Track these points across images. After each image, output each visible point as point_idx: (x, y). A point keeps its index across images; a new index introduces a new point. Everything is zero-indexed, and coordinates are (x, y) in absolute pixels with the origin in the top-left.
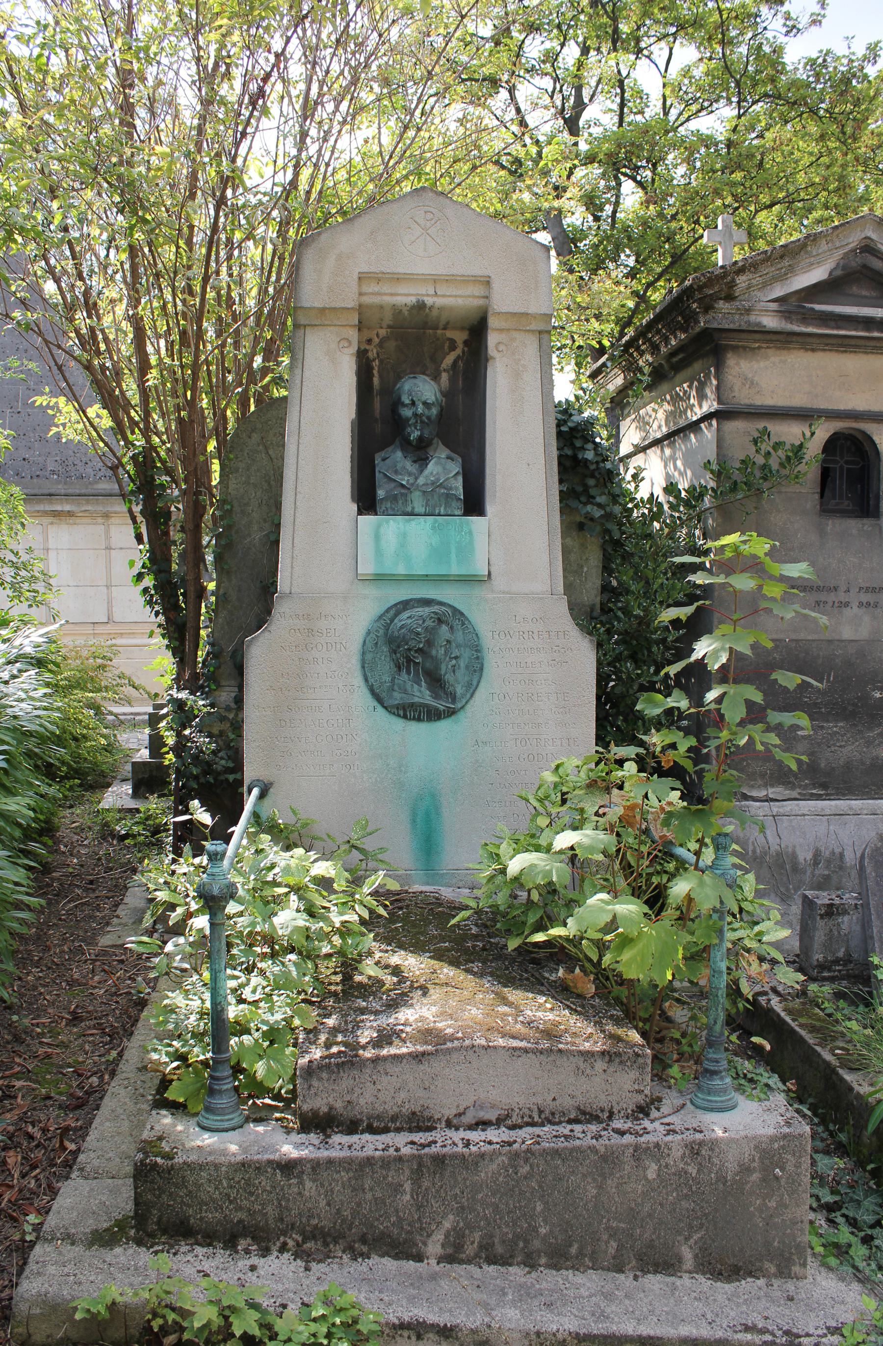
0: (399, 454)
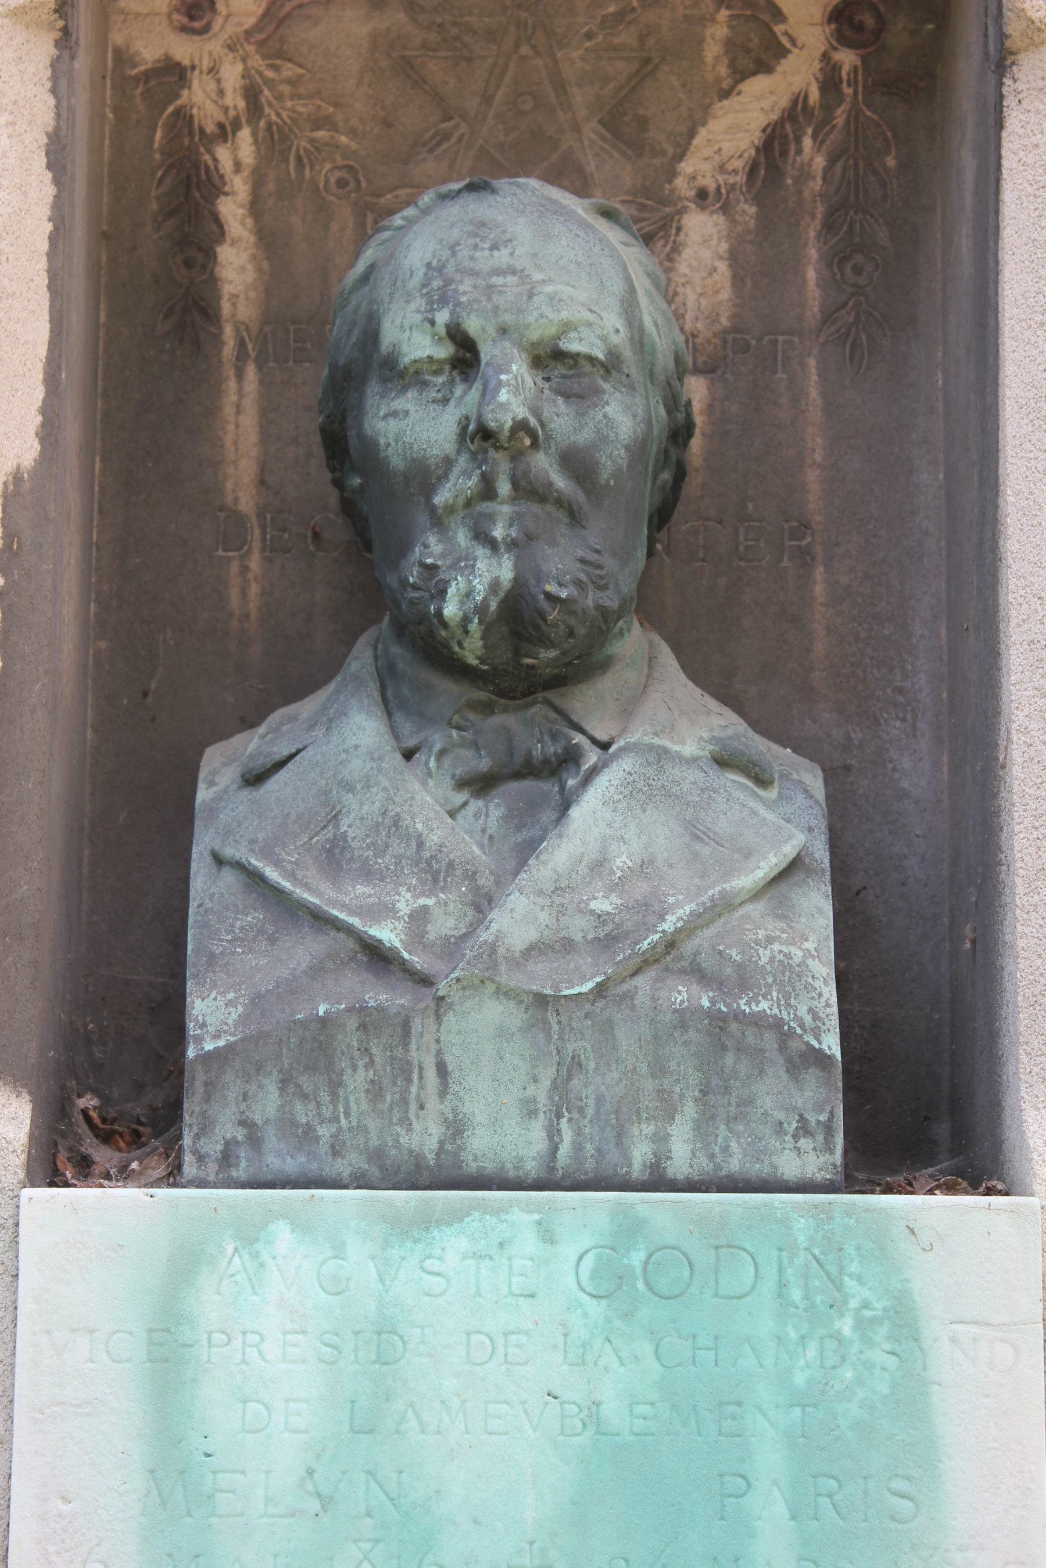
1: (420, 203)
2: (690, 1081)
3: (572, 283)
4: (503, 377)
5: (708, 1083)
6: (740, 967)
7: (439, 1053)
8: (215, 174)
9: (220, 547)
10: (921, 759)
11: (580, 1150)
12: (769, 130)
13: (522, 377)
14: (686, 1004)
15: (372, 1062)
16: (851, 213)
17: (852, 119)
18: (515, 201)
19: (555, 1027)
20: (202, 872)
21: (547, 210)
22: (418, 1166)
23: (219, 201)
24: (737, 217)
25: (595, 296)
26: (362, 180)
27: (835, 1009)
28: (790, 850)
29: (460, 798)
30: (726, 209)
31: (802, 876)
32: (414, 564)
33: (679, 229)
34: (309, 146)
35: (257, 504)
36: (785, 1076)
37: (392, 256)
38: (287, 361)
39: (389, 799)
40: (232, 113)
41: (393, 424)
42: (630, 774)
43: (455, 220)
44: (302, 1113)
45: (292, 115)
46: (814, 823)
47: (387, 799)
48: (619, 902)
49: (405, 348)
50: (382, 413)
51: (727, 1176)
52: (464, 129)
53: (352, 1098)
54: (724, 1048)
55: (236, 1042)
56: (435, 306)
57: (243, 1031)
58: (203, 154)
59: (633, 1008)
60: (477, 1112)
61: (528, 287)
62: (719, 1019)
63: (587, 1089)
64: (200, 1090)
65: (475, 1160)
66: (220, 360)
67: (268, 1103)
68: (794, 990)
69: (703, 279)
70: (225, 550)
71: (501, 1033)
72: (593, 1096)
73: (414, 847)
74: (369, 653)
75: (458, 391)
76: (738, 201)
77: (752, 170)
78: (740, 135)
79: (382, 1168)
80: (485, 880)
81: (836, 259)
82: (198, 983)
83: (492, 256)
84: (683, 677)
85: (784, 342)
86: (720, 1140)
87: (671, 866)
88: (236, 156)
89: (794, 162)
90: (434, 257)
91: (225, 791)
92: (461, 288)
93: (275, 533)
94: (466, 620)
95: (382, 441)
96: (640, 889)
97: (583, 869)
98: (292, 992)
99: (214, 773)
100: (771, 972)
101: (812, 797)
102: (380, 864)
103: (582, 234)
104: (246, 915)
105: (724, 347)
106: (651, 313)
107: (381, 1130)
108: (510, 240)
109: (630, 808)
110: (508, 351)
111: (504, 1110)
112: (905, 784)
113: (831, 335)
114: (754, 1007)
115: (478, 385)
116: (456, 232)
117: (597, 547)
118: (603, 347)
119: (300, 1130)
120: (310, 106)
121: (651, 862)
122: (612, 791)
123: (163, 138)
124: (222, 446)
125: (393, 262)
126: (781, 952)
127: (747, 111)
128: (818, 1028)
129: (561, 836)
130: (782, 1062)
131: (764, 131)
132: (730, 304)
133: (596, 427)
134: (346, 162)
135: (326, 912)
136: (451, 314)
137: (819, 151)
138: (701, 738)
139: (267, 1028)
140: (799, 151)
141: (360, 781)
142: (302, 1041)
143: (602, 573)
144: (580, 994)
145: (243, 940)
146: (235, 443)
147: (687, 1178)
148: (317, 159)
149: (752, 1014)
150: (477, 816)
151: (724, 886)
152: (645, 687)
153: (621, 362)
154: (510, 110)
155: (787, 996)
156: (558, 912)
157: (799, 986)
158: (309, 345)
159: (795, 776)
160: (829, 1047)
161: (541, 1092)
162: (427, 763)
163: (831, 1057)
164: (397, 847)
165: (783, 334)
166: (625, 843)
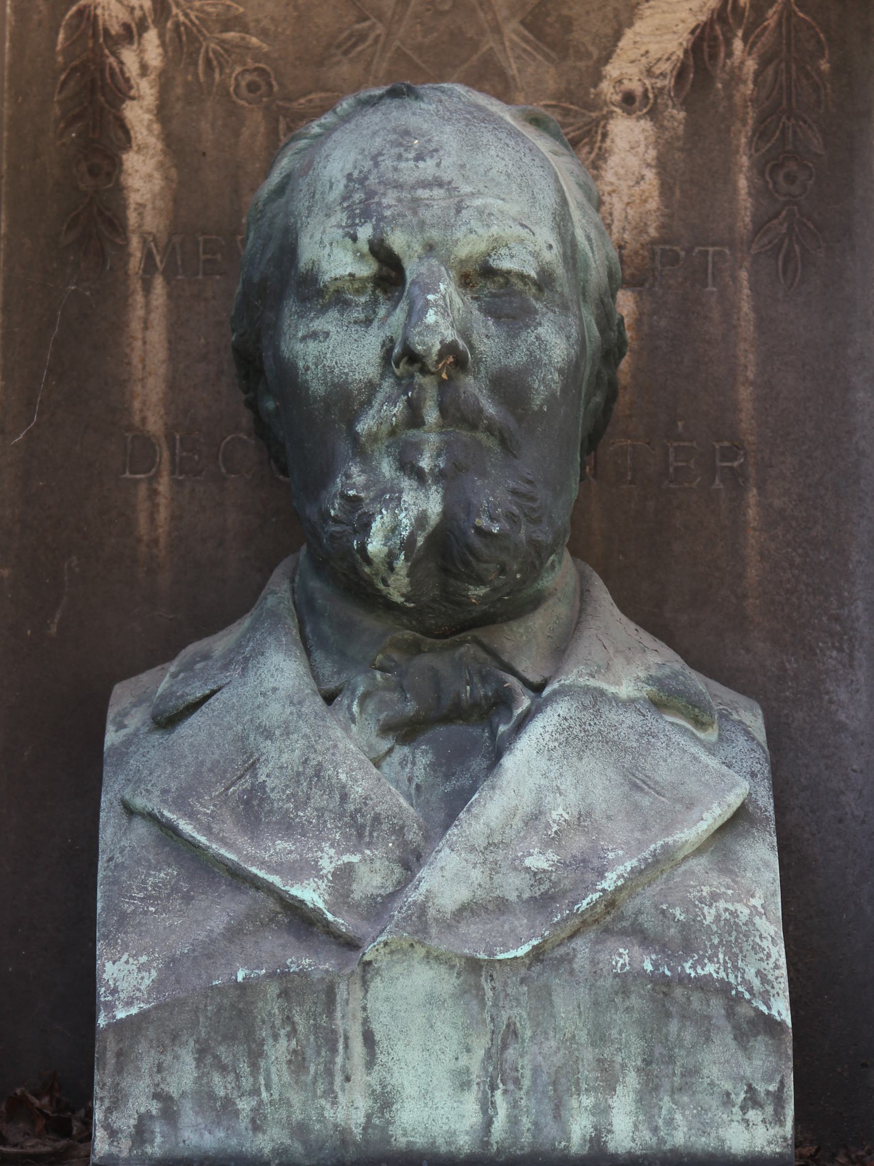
0: (282, 670)
1: (338, 110)
2: (632, 1049)
3: (503, 196)
4: (431, 297)
5: (651, 1053)
6: (684, 927)
7: (366, 1021)
8: (120, 77)
9: (127, 470)
10: (858, 691)
11: (516, 1124)
12: (698, 31)
13: (450, 297)
14: (628, 968)
15: (294, 1031)
16: (784, 119)
17: (784, 20)
18: (440, 108)
19: (490, 994)
20: (112, 821)
21: (474, 117)
22: (343, 1141)
23: (124, 106)
24: (666, 123)
25: (526, 210)
26: (274, 83)
27: (784, 971)
28: (734, 800)
29: (384, 745)
30: (653, 114)
31: (747, 826)
32: (335, 495)
33: (605, 135)
34: (218, 48)
35: (166, 424)
36: (732, 1044)
37: (310, 165)
38: (197, 274)
39: (310, 747)
40: (138, 13)
41: (312, 347)
42: (566, 719)
43: (377, 128)
44: (220, 1085)
45: (201, 15)
46: (757, 767)
47: (308, 747)
48: (556, 858)
49: (325, 266)
50: (300, 334)
51: (671, 1151)
52: (380, 29)
53: (273, 1069)
54: (668, 1015)
55: (149, 1010)
56: (357, 221)
57: (157, 998)
58: (108, 57)
59: (572, 972)
60: (405, 1083)
61: (457, 200)
62: (663, 984)
63: (524, 1058)
64: (111, 1060)
65: (404, 1135)
66: (126, 273)
67: (184, 1075)
68: (741, 952)
69: (630, 187)
70: (133, 472)
71: (432, 1000)
72: (529, 1067)
73: (338, 799)
74: (286, 585)
75: (382, 312)
76: (667, 106)
77: (681, 75)
78: (669, 36)
79: (305, 1143)
80: (413, 835)
81: (769, 166)
82: (108, 945)
83: (417, 167)
84: (616, 611)
85: (715, 254)
86: (664, 1112)
87: (609, 818)
88: (142, 59)
89: (725, 65)
90: (355, 168)
91: (135, 734)
92: (385, 201)
93: (184, 454)
94: (391, 557)
95: (301, 364)
96: (578, 844)
97: (517, 822)
98: (209, 956)
99: (125, 714)
100: (716, 932)
101: (753, 739)
102: (301, 817)
103: (512, 143)
104: (159, 871)
105: (653, 259)
106: (582, 227)
107: (304, 1103)
108: (436, 150)
109: (565, 756)
110: (435, 269)
111: (435, 1082)
112: (842, 717)
113: (763, 247)
114: (699, 971)
115: (403, 305)
116: (378, 141)
117: (530, 477)
118: (535, 265)
119: (219, 1104)
120: (220, 6)
121: (589, 814)
122: (547, 739)
123: (66, 39)
124: (129, 363)
125: (311, 172)
126: (726, 910)
127: (675, 12)
128: (767, 992)
129: (493, 788)
130: (729, 1029)
131: (693, 32)
132: (658, 213)
133: (528, 350)
134: (257, 65)
135: (244, 870)
136: (374, 229)
137: (749, 54)
138: (638, 677)
139: (182, 995)
140: (730, 54)
141: (279, 727)
142: (220, 1008)
143: (535, 506)
144: (516, 958)
145: (157, 898)
146: (143, 360)
147: (629, 1153)
148: (227, 62)
149: (698, 979)
150: (403, 763)
151: (666, 840)
152: (578, 623)
153: (554, 280)
154: (428, 10)
155: (734, 957)
156: (492, 869)
157: (746, 947)
158: (219, 257)
159: (735, 717)
160: (779, 1012)
161: (475, 1062)
162: (349, 707)
163: (781, 1024)
164: (319, 799)
165: (713, 245)
166: (561, 794)
